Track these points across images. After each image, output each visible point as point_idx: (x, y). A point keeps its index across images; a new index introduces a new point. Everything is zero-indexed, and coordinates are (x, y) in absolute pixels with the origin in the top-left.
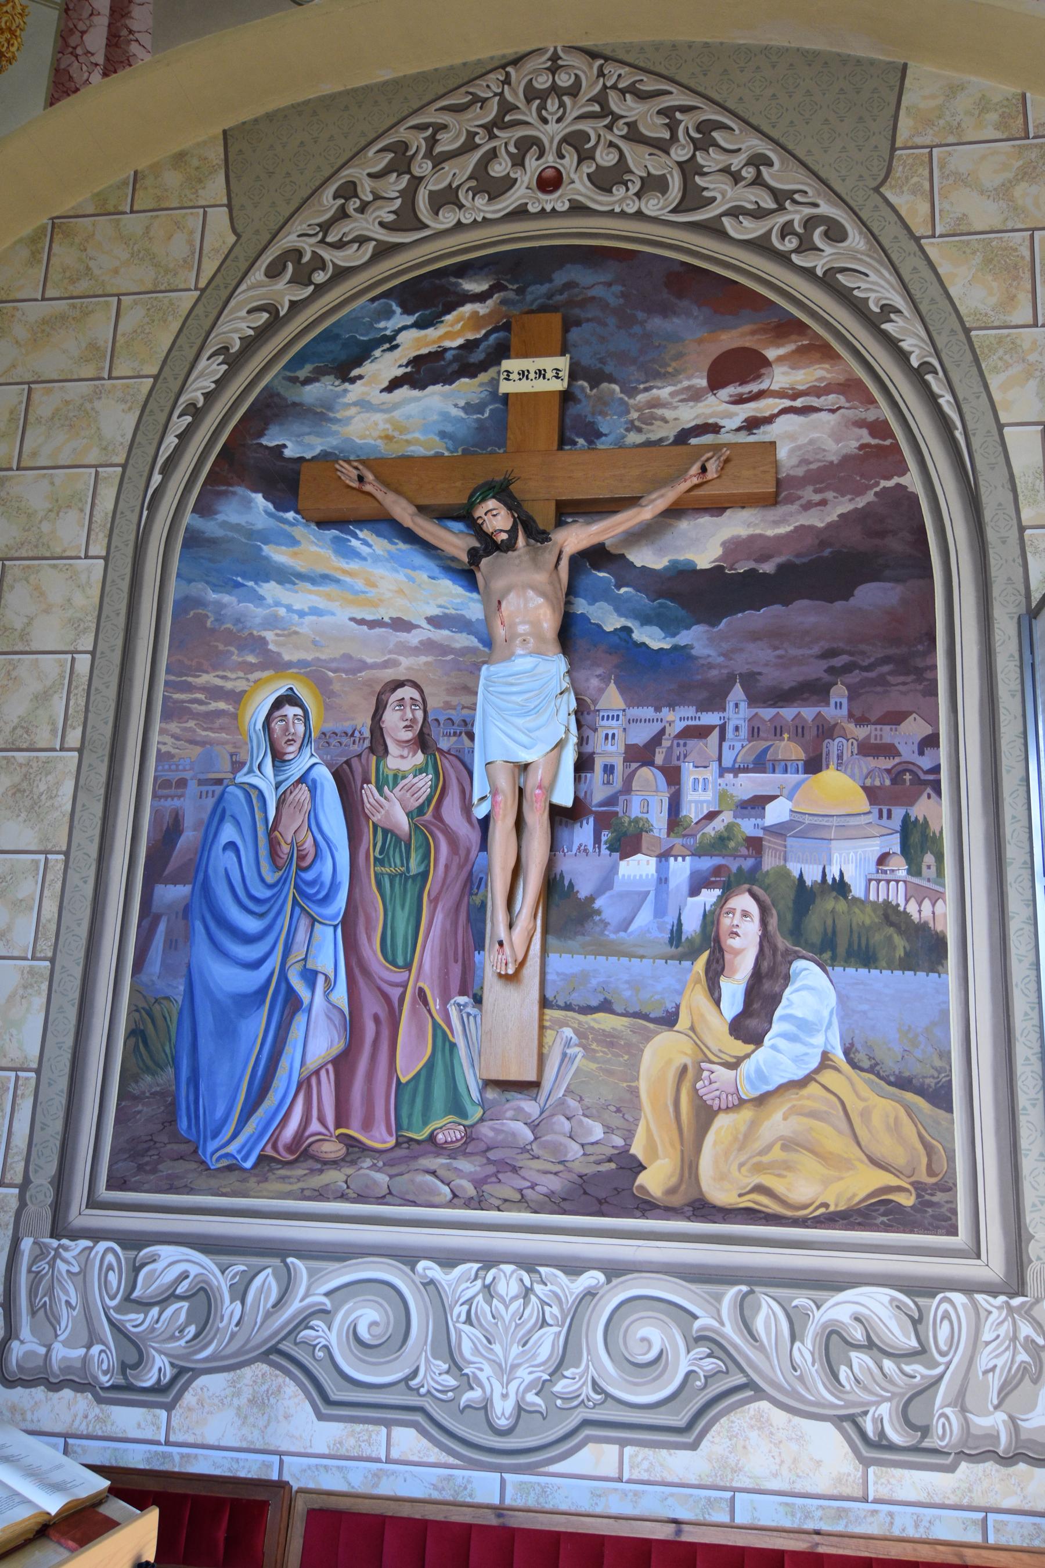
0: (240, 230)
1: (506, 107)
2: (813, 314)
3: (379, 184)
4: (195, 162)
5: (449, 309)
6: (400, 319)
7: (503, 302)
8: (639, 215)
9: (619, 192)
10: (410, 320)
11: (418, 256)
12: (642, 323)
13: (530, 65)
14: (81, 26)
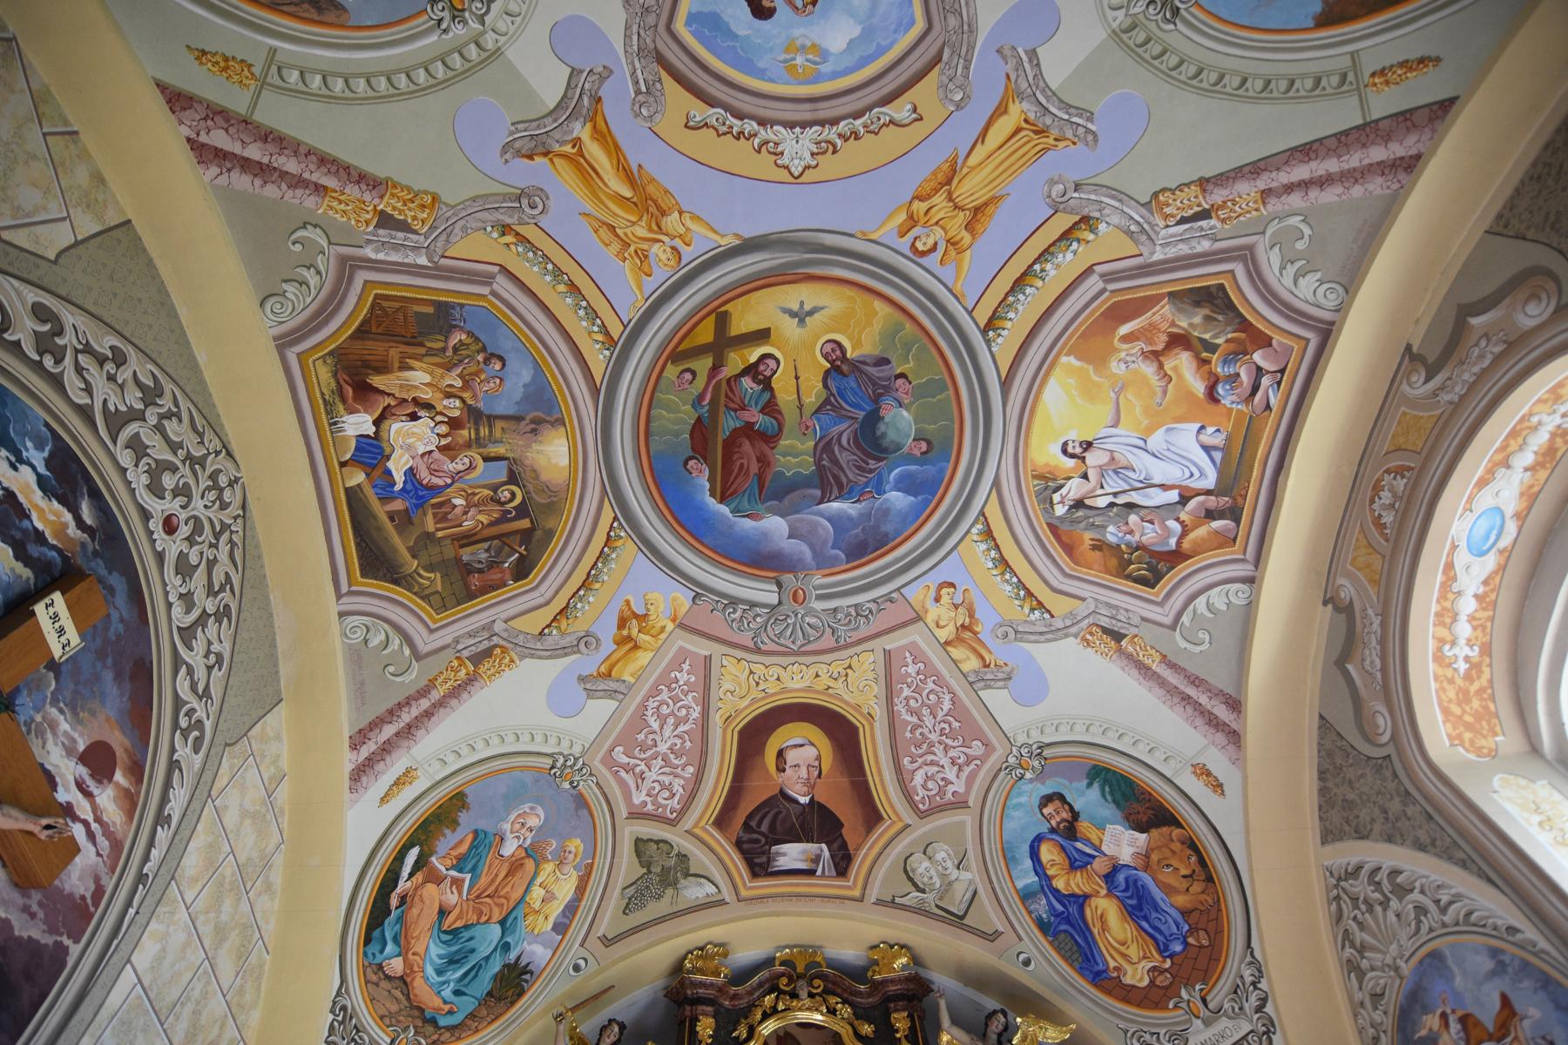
0: (61, 261)
1: (202, 461)
2: (151, 777)
3: (131, 384)
4: (100, 197)
5: (62, 501)
6: (38, 458)
7: (83, 545)
8: (169, 605)
9: (178, 581)
10: (42, 470)
11: (90, 446)
12: (105, 666)
13: (229, 465)
14: (232, 130)
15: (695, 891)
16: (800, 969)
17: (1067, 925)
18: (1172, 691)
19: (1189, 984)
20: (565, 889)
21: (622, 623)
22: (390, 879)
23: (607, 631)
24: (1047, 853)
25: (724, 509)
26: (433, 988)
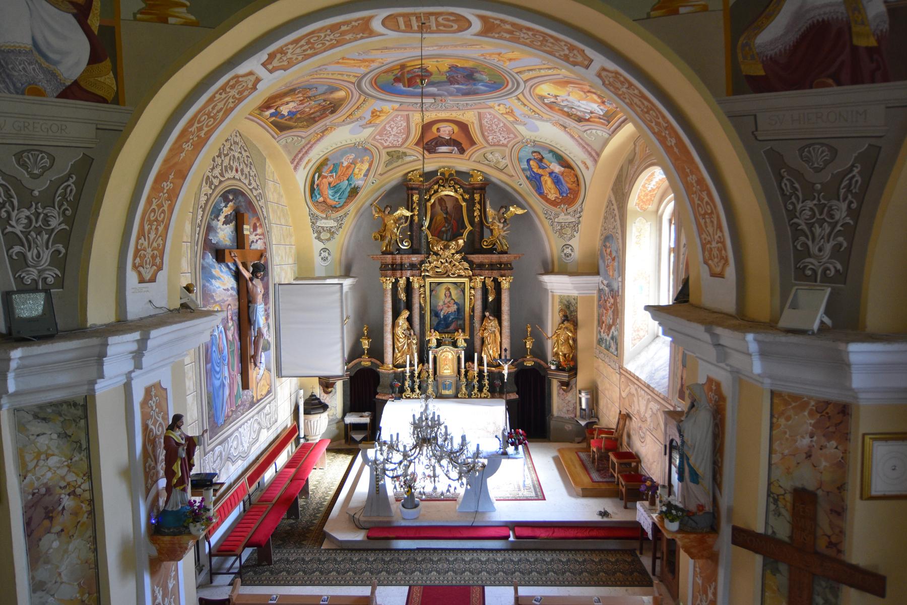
15: (408, 159)
16: (447, 176)
17: (535, 180)
18: (580, 144)
19: (564, 204)
20: (365, 167)
21: (373, 113)
22: (313, 182)
23: (368, 116)
24: (531, 163)
25: (410, 89)
26: (332, 199)
